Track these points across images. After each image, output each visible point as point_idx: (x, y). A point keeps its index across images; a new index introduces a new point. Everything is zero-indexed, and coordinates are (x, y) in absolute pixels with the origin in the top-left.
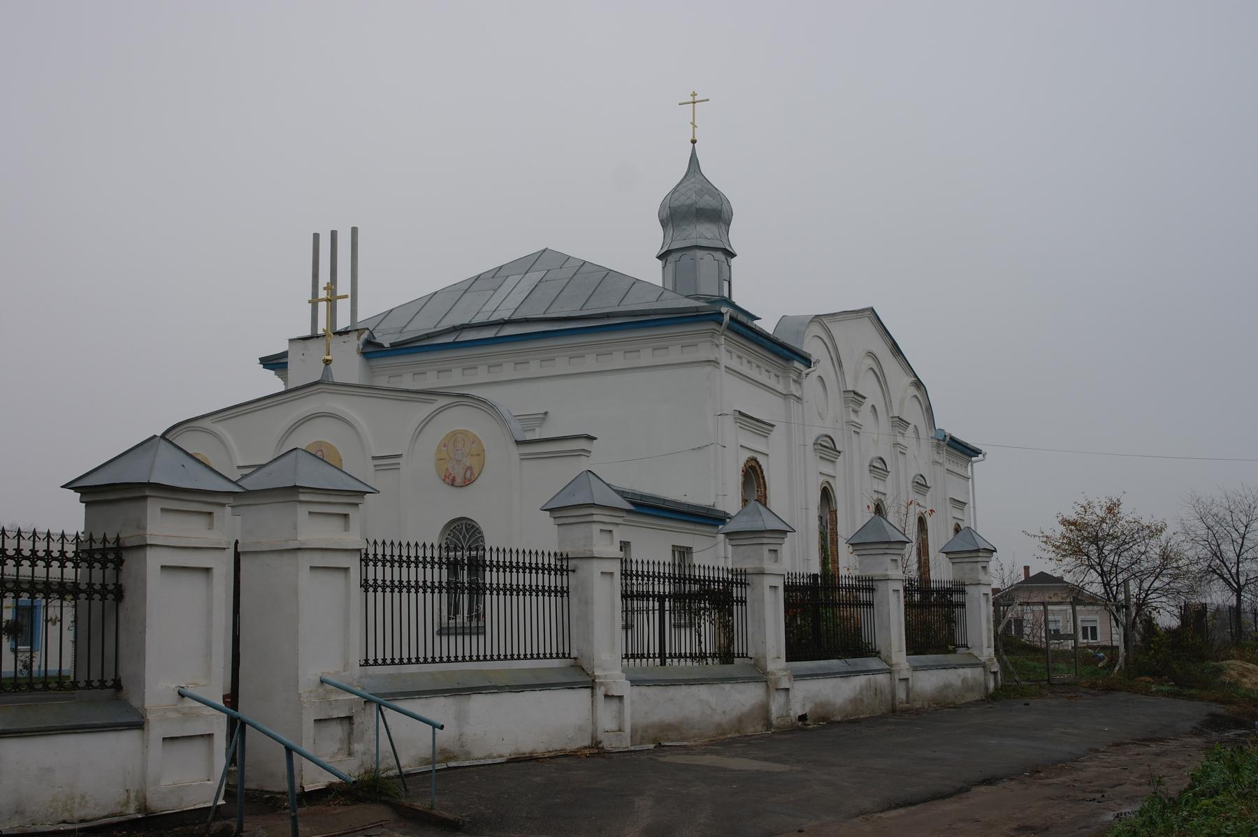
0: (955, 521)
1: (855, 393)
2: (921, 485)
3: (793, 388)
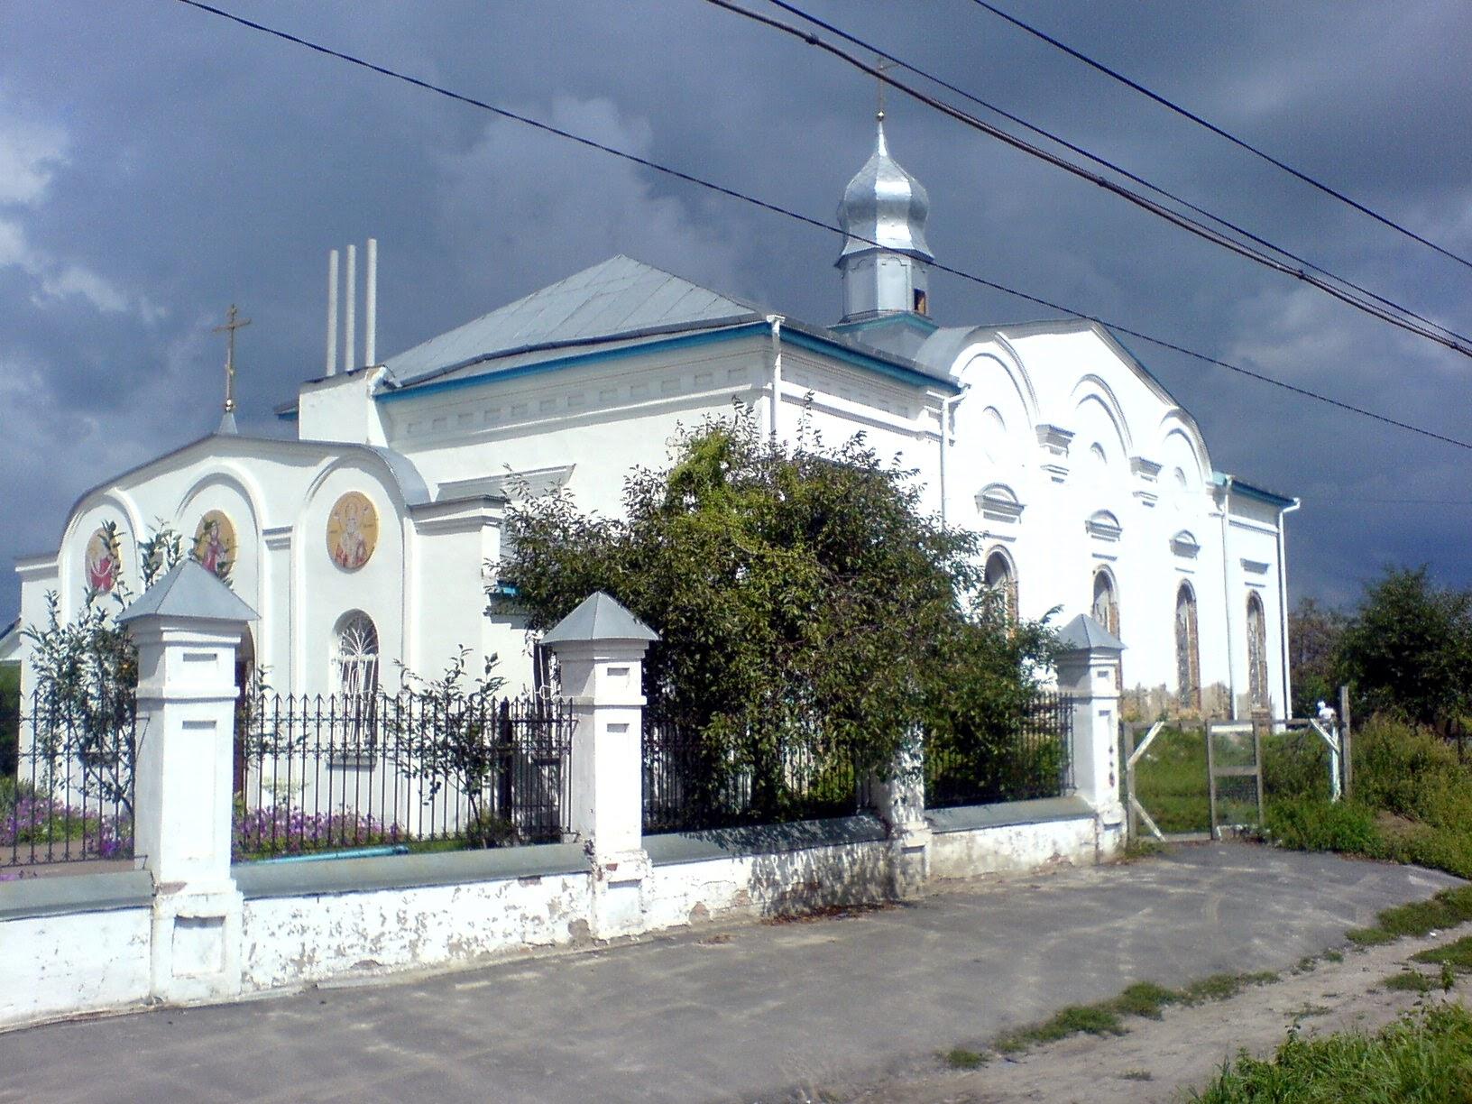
0: (1248, 589)
2: (1185, 548)
3: (932, 425)
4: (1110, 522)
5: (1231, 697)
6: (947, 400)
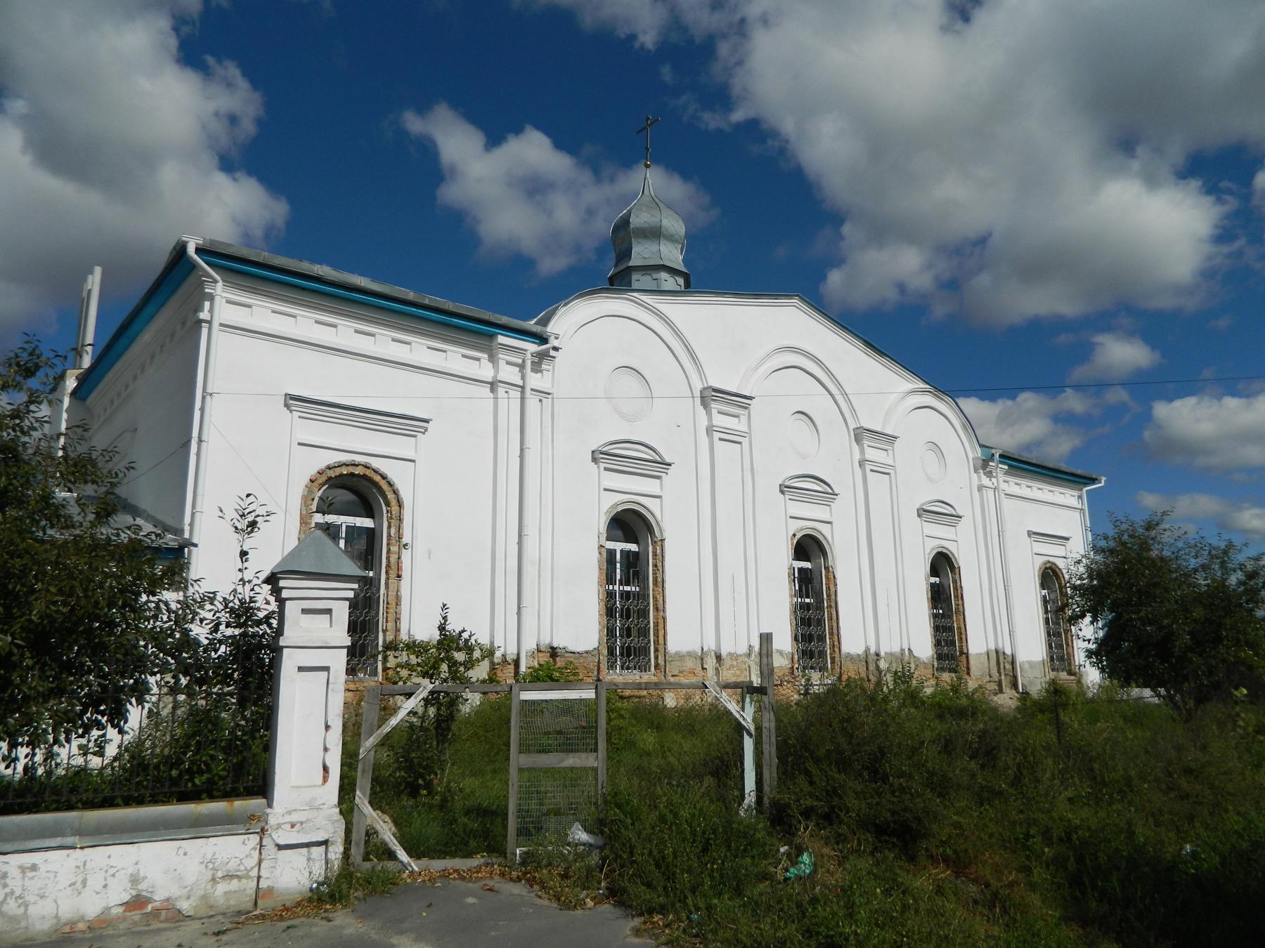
1: (715, 390)
4: (948, 510)
5: (1013, 663)
6: (532, 347)
